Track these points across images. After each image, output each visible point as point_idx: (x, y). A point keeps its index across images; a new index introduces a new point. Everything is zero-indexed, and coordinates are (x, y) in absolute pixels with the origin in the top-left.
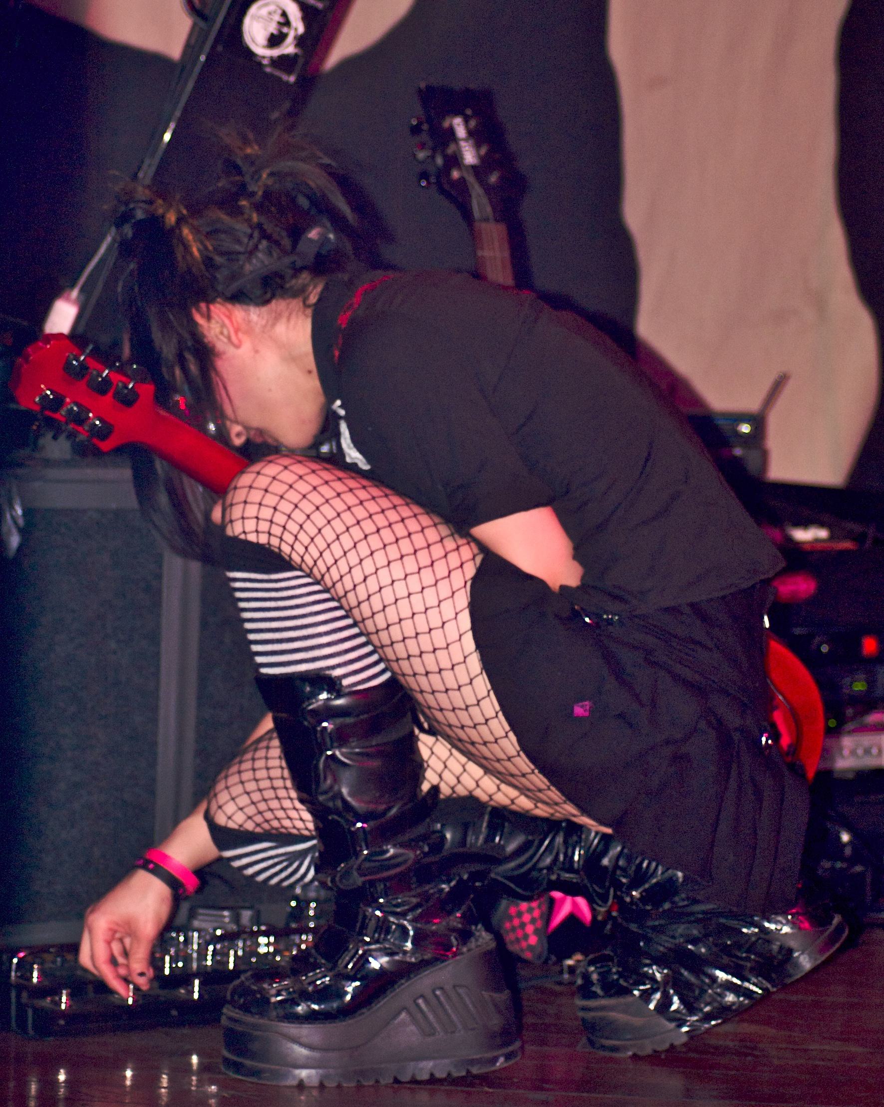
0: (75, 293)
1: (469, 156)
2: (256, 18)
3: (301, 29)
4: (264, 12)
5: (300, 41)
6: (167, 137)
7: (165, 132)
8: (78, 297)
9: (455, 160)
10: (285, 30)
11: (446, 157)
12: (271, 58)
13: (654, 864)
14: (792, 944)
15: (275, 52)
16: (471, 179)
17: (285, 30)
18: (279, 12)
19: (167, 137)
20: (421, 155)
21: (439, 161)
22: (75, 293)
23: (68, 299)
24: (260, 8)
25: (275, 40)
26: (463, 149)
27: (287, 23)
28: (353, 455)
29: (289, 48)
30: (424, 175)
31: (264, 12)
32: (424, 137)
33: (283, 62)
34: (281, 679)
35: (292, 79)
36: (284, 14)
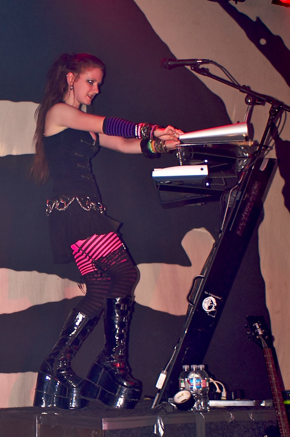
0: (165, 371)
1: (260, 333)
2: (205, 302)
3: (216, 305)
4: (207, 301)
5: (216, 307)
6: (186, 332)
7: (186, 333)
8: (166, 373)
9: (257, 334)
10: (212, 305)
11: (254, 333)
12: (209, 312)
13: (103, 268)
14: (116, 308)
15: (210, 310)
16: (261, 338)
17: (212, 305)
18: (211, 300)
19: (186, 332)
20: (248, 333)
21: (253, 334)
22: (165, 371)
23: (163, 373)
24: (206, 300)
25: (210, 308)
26: (258, 331)
27: (212, 303)
28: (189, 67)
29: (213, 309)
30: (250, 338)
31: (207, 301)
32: (249, 328)
33: (212, 313)
34: (249, 399)
35: (214, 317)
36: (212, 301)
